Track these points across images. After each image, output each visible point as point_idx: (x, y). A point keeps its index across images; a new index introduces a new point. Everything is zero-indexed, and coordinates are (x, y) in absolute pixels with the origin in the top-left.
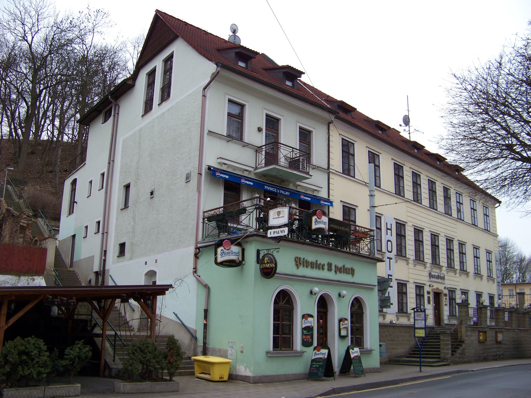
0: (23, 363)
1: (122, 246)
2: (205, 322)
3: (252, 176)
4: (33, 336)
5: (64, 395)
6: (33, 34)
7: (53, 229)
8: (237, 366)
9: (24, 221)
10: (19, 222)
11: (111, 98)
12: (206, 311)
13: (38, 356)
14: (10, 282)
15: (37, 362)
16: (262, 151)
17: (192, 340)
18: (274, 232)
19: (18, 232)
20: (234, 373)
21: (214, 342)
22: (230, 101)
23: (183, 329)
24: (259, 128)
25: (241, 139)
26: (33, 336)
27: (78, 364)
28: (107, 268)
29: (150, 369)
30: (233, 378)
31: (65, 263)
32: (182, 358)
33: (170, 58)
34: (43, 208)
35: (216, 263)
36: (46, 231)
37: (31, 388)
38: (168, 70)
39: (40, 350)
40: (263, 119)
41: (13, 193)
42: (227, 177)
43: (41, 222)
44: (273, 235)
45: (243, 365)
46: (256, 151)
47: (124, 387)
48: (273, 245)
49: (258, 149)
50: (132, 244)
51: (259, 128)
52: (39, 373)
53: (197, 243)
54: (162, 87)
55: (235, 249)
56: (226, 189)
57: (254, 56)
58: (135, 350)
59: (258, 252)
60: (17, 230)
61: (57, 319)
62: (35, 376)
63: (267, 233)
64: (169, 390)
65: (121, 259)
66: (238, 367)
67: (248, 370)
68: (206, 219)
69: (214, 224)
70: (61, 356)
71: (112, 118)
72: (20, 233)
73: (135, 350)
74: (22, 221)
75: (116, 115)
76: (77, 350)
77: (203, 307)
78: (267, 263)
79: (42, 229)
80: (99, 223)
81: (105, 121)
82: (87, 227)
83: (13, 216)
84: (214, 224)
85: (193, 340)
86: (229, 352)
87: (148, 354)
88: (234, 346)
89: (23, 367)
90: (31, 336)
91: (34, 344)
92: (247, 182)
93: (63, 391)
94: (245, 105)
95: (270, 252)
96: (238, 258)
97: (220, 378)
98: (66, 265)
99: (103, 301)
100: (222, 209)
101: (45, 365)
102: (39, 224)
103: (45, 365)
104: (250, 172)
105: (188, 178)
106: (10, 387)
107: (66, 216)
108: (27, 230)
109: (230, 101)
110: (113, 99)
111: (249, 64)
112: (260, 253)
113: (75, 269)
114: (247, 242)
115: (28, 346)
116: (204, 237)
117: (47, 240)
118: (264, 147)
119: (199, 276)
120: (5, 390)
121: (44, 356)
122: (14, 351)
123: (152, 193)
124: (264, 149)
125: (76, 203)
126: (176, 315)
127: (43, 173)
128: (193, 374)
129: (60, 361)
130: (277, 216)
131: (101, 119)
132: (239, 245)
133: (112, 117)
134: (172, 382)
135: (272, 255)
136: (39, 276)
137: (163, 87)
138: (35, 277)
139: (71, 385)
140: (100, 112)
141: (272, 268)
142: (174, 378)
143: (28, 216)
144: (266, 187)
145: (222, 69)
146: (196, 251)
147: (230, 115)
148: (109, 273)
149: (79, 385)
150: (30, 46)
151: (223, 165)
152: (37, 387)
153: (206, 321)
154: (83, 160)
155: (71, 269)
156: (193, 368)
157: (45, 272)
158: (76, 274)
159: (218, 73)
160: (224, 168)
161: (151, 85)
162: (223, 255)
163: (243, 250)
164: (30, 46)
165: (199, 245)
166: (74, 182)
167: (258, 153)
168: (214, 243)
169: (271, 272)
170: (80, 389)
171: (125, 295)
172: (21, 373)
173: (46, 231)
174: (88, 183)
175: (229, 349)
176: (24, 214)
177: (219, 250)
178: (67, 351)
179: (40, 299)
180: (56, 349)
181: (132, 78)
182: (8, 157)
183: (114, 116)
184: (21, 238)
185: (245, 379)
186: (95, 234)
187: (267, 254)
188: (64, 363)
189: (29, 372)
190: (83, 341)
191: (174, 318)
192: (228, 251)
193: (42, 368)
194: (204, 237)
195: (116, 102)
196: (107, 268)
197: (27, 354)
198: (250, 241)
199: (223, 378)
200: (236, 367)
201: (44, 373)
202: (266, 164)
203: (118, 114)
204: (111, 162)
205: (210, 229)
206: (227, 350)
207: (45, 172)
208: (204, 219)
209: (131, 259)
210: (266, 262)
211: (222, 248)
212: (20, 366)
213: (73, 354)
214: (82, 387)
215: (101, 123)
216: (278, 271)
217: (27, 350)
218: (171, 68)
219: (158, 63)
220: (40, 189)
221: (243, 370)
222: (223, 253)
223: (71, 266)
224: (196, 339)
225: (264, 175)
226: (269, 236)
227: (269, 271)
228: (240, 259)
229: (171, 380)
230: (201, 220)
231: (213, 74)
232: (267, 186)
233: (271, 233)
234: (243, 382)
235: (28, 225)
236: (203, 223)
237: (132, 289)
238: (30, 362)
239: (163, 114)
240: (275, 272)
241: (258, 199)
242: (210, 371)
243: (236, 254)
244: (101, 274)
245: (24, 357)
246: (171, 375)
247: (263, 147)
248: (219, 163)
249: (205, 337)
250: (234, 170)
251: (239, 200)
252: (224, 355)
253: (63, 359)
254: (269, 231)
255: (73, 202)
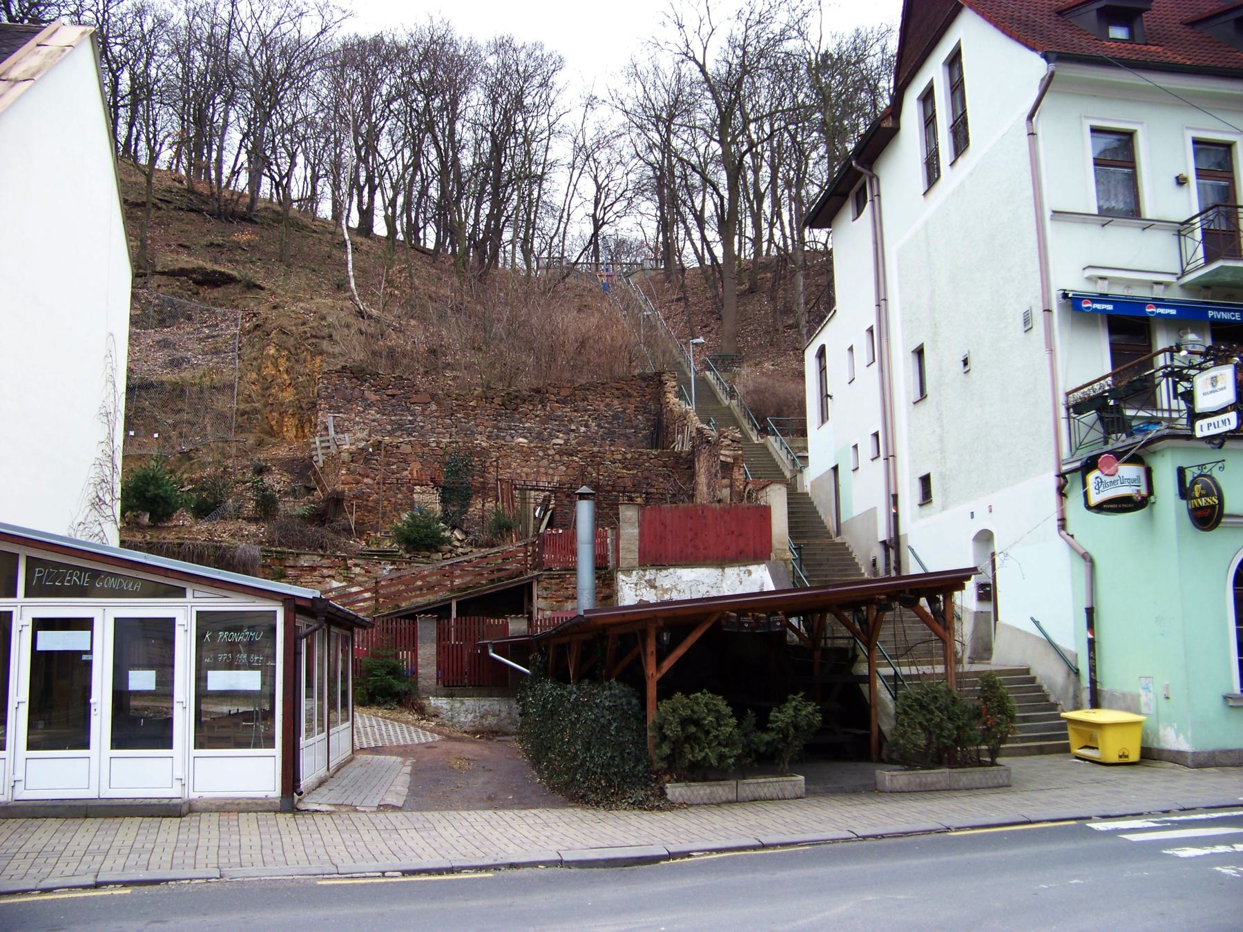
0: (690, 739)
1: (925, 481)
2: (1090, 636)
3: (1176, 294)
4: (705, 690)
5: (775, 796)
6: (705, 41)
7: (798, 457)
8: (1161, 728)
9: (727, 453)
10: (717, 456)
11: (858, 163)
12: (1090, 612)
13: (715, 725)
14: (707, 581)
15: (716, 737)
16: (1192, 231)
17: (1069, 674)
18: (1209, 425)
19: (719, 475)
20: (1155, 745)
21: (1110, 681)
22: (1094, 130)
23: (1053, 655)
24: (1177, 178)
25: (1133, 212)
26: (705, 690)
27: (795, 738)
28: (902, 532)
29: (944, 743)
30: (1150, 755)
31: (825, 527)
32: (1012, 718)
33: (954, 61)
34: (779, 413)
35: (1088, 507)
36: (786, 461)
37: (713, 783)
38: (957, 87)
39: (719, 718)
40: (1185, 154)
41: (718, 388)
42: (1110, 307)
43: (773, 443)
44: (1207, 433)
45: (1172, 727)
46: (1179, 234)
47: (892, 781)
48: (1208, 456)
49: (1181, 228)
50: (943, 476)
51: (1177, 178)
52: (722, 758)
53: (1059, 462)
54: (951, 123)
55: (1129, 471)
56: (1113, 330)
57: (1145, 6)
58: (908, 706)
59: (1181, 472)
60: (717, 471)
61: (795, 648)
62: (714, 762)
63: (1193, 429)
64: (990, 784)
65: (927, 508)
66: (1161, 733)
67: (1181, 738)
68: (1071, 410)
69: (1090, 417)
70: (762, 724)
71: (868, 205)
72: (723, 478)
73: (909, 706)
74: (722, 452)
75: (876, 198)
76: (791, 712)
77: (1083, 604)
78: (1201, 496)
79: (777, 459)
80: (876, 435)
81: (859, 212)
82: (855, 447)
83: (708, 442)
84: (1090, 417)
85: (1073, 676)
86: (1143, 699)
87: (937, 713)
88: (1150, 685)
89: (692, 748)
90: (700, 691)
91: (706, 705)
92: (1162, 311)
93: (771, 789)
94: (1135, 131)
95: (1205, 471)
96: (1138, 491)
97: (1120, 757)
98: (828, 532)
99: (864, 608)
100: (1110, 378)
101: (729, 742)
102: (771, 449)
103: (729, 742)
104: (1167, 285)
105: (1027, 320)
106: (677, 781)
107: (816, 426)
108: (736, 469)
109: (1094, 130)
110: (863, 166)
111: (1137, 30)
112: (1185, 476)
113: (845, 538)
114: (1154, 453)
115: (696, 708)
116: (1074, 450)
117: (768, 489)
118: (1198, 219)
119: (1072, 536)
120: (668, 785)
121: (726, 725)
122: (671, 718)
123: (965, 362)
124: (1198, 225)
125: (830, 397)
126: (1037, 623)
127: (777, 330)
128: (1066, 749)
129: (759, 733)
130: (1210, 388)
131: (849, 210)
132: (1136, 460)
133: (868, 205)
134: (994, 768)
135: (1210, 477)
136: (759, 564)
137: (955, 122)
138: (752, 568)
139: (785, 779)
140: (844, 197)
141: (1212, 507)
142: (999, 760)
143: (733, 441)
144: (1210, 313)
145: (1059, 64)
146: (1060, 481)
147: (1099, 162)
148: (906, 540)
149: (801, 778)
150: (702, 69)
151: (1100, 281)
152: (722, 783)
153: (1093, 633)
154: (830, 303)
155: (838, 540)
156: (1066, 737)
157: (772, 555)
158: (848, 549)
159: (1052, 76)
160: (1102, 288)
161: (930, 121)
162: (1100, 487)
163: (1149, 473)
164: (702, 69)
165: (1065, 468)
166: (822, 353)
167: (1182, 238)
168: (1078, 464)
169: (1211, 515)
170: (803, 786)
171: (883, 597)
172: (690, 756)
173: (786, 461)
174: (847, 353)
175: (1142, 692)
176: (725, 437)
177: (1092, 477)
178: (773, 714)
179: (714, 619)
180: (749, 712)
181: (891, 114)
182: (704, 309)
183: (872, 200)
184: (727, 487)
185: (1177, 758)
186: (873, 460)
187: (1200, 475)
188: (767, 737)
189: (703, 754)
190: (802, 694)
191: (1033, 629)
192: (1112, 479)
193: (725, 747)
194: (1074, 450)
195: (870, 170)
196: (902, 532)
197: (697, 723)
198: (1159, 451)
199: (1127, 757)
200: (1158, 730)
201: (731, 757)
202: (1209, 259)
203: (879, 195)
204: (881, 302)
205: (1084, 430)
206: (1139, 696)
207: (781, 329)
208: (1068, 409)
209: (944, 508)
210: (1197, 495)
211: (1096, 473)
212: (687, 745)
213: (782, 721)
214: (806, 780)
215: (851, 218)
216: (1227, 510)
217: (695, 717)
218: (962, 81)
219: (934, 71)
220: (774, 370)
221: (1173, 739)
222: (1100, 484)
223: (838, 533)
224: (1077, 672)
225: (1204, 286)
226: (1199, 434)
227: (1207, 514)
228: (1144, 492)
229: (993, 764)
230: (1063, 412)
231: (1042, 80)
232: (1213, 310)
233: (1203, 429)
234: (1171, 764)
235: (736, 458)
236: (1069, 418)
237: (941, 579)
238: (703, 737)
239: (962, 185)
240: (1221, 514)
241: (1168, 354)
242: (1096, 741)
243: (1131, 482)
244: (893, 545)
245: (693, 729)
246: (994, 753)
247: (1194, 221)
248: (1089, 279)
249: (1093, 669)
250: (1128, 287)
251: (1150, 351)
252: (1133, 708)
253: (767, 730)
254: (1198, 424)
255: (825, 396)
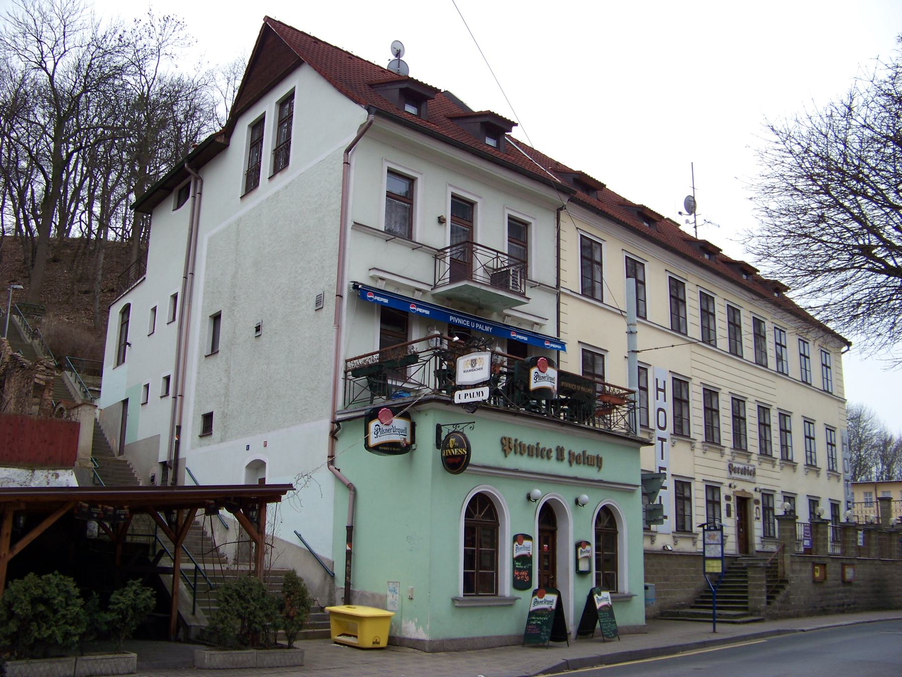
0: (40, 618)
1: (208, 418)
2: (348, 548)
3: (429, 300)
4: (56, 572)
5: (109, 671)
6: (57, 58)
7: (90, 390)
8: (403, 622)
9: (41, 377)
10: (32, 378)
11: (189, 166)
12: (350, 530)
13: (64, 605)
14: (17, 479)
15: (64, 616)
16: (444, 258)
17: (325, 578)
18: (466, 395)
19: (31, 395)
20: (398, 634)
21: (363, 582)
22: (390, 172)
23: (311, 559)
24: (439, 218)
25: (409, 236)
26: (56, 572)
27: (132, 619)
28: (181, 456)
29: (255, 628)
30: (395, 643)
31: (110, 447)
32: (309, 609)
33: (289, 98)
34: (74, 354)
35: (367, 447)
36: (79, 392)
37: (53, 660)
38: (285, 120)
39: (68, 595)
40: (446, 202)
41: (22, 328)
42: (386, 301)
43: (69, 377)
44: (463, 400)
45: (413, 621)
46: (436, 257)
47: (210, 659)
48: (464, 416)
49: (438, 254)
50: (224, 415)
51: (439, 218)
52: (67, 635)
53: (334, 413)
54: (275, 147)
55: (399, 423)
56: (383, 321)
57: (431, 96)
58: (229, 595)
59: (439, 428)
60: (29, 391)
61: (97, 542)
62: (60, 640)
63: (453, 397)
64: (288, 664)
65: (206, 440)
66: (404, 625)
67: (421, 629)
68: (350, 373)
69: (363, 380)
70: (104, 605)
71: (190, 201)
72: (35, 397)
73: (230, 596)
74: (37, 375)
75: (198, 196)
76: (132, 595)
77: (345, 523)
78: (454, 447)
79: (71, 390)
80: (168, 379)
81: (179, 205)
82: (147, 386)
83: (22, 367)
84: (363, 380)
85: (329, 578)
86: (390, 599)
87: (252, 602)
88: (397, 588)
89: (38, 625)
90: (52, 572)
91: (57, 586)
92: (420, 310)
93: (107, 665)
94: (417, 178)
95: (458, 429)
96: (405, 439)
97: (374, 643)
98: (111, 451)
99: (175, 511)
100: (378, 355)
101: (76, 622)
102: (66, 381)
103: (76, 622)
104: (424, 292)
105: (319, 303)
106: (17, 658)
107: (112, 367)
108: (46, 391)
109: (390, 172)
110: (192, 169)
111: (423, 110)
112: (441, 431)
113: (127, 457)
114: (419, 411)
115: (47, 588)
116: (347, 404)
117: (80, 409)
118: (449, 250)
119: (339, 470)
120: (8, 663)
121: (74, 605)
122: (23, 598)
123: (258, 329)
124: (449, 254)
125: (129, 345)
126: (299, 536)
127: (73, 293)
128: (328, 636)
129: (103, 614)
130: (470, 368)
131: (171, 202)
132: (406, 416)
133: (190, 199)
134: (292, 650)
135: (462, 433)
136: (66, 469)
137: (278, 147)
138: (60, 472)
139: (120, 655)
140: (169, 191)
141: (462, 456)
142: (296, 644)
143: (47, 368)
144: (451, 318)
145: (377, 117)
146: (333, 427)
147: (391, 195)
148: (185, 464)
149: (135, 655)
150: (51, 78)
151: (379, 280)
152: (62, 659)
153: (351, 546)
154: (141, 272)
155: (121, 458)
156: (328, 626)
157: (77, 463)
158: (129, 466)
159: (370, 123)
160: (381, 285)
161: (256, 144)
162: (378, 433)
163: (413, 426)
164: (51, 78)
165: (338, 417)
166: (126, 310)
167: (438, 261)
168: (363, 413)
169: (460, 463)
170: (135, 662)
171: (213, 502)
172: (36, 634)
173: (79, 392)
174: (150, 312)
175: (389, 593)
176: (41, 364)
177: (373, 425)
178: (114, 597)
179: (68, 508)
180: (94, 594)
181: (224, 133)
182: (13, 268)
183: (194, 197)
184: (36, 404)
185: (416, 645)
186: (161, 397)
187: (454, 432)
188: (109, 617)
189: (50, 632)
190: (140, 580)
191: (295, 541)
192: (388, 427)
193: (71, 625)
194: (347, 404)
195: (197, 173)
196: (182, 455)
197: (46, 602)
198: (424, 411)
199: (378, 643)
200: (401, 624)
201: (75, 635)
202: (453, 280)
203: (200, 194)
204: (189, 275)
205: (357, 389)
206: (386, 596)
207: (76, 293)
208: (346, 372)
209: (222, 441)
210: (451, 446)
211: (377, 422)
212: (34, 623)
213: (124, 603)
214: (140, 658)
215: (172, 209)
216: (472, 460)
217: (46, 596)
218: (291, 116)
219: (268, 107)
220: (69, 322)
221: (413, 630)
222: (378, 431)
223: (121, 452)
224: (333, 576)
225: (448, 297)
226: (457, 401)
227: (457, 460)
228: (408, 441)
229: (290, 647)
230: (341, 375)
231: (362, 126)
232: (453, 316)
233: (460, 397)
234: (412, 650)
235: (47, 382)
236: (346, 379)
237: (224, 492)
238: (51, 615)
239: (277, 194)
240: (467, 463)
241: (439, 339)
242: (356, 631)
243: (401, 432)
244: (172, 465)
245: (41, 608)
246: (291, 638)
247: (447, 251)
248: (372, 277)
249: (348, 574)
250: (398, 289)
251: (406, 340)
252: (380, 603)
253: (106, 610)
254: (457, 393)
255: (123, 344)
